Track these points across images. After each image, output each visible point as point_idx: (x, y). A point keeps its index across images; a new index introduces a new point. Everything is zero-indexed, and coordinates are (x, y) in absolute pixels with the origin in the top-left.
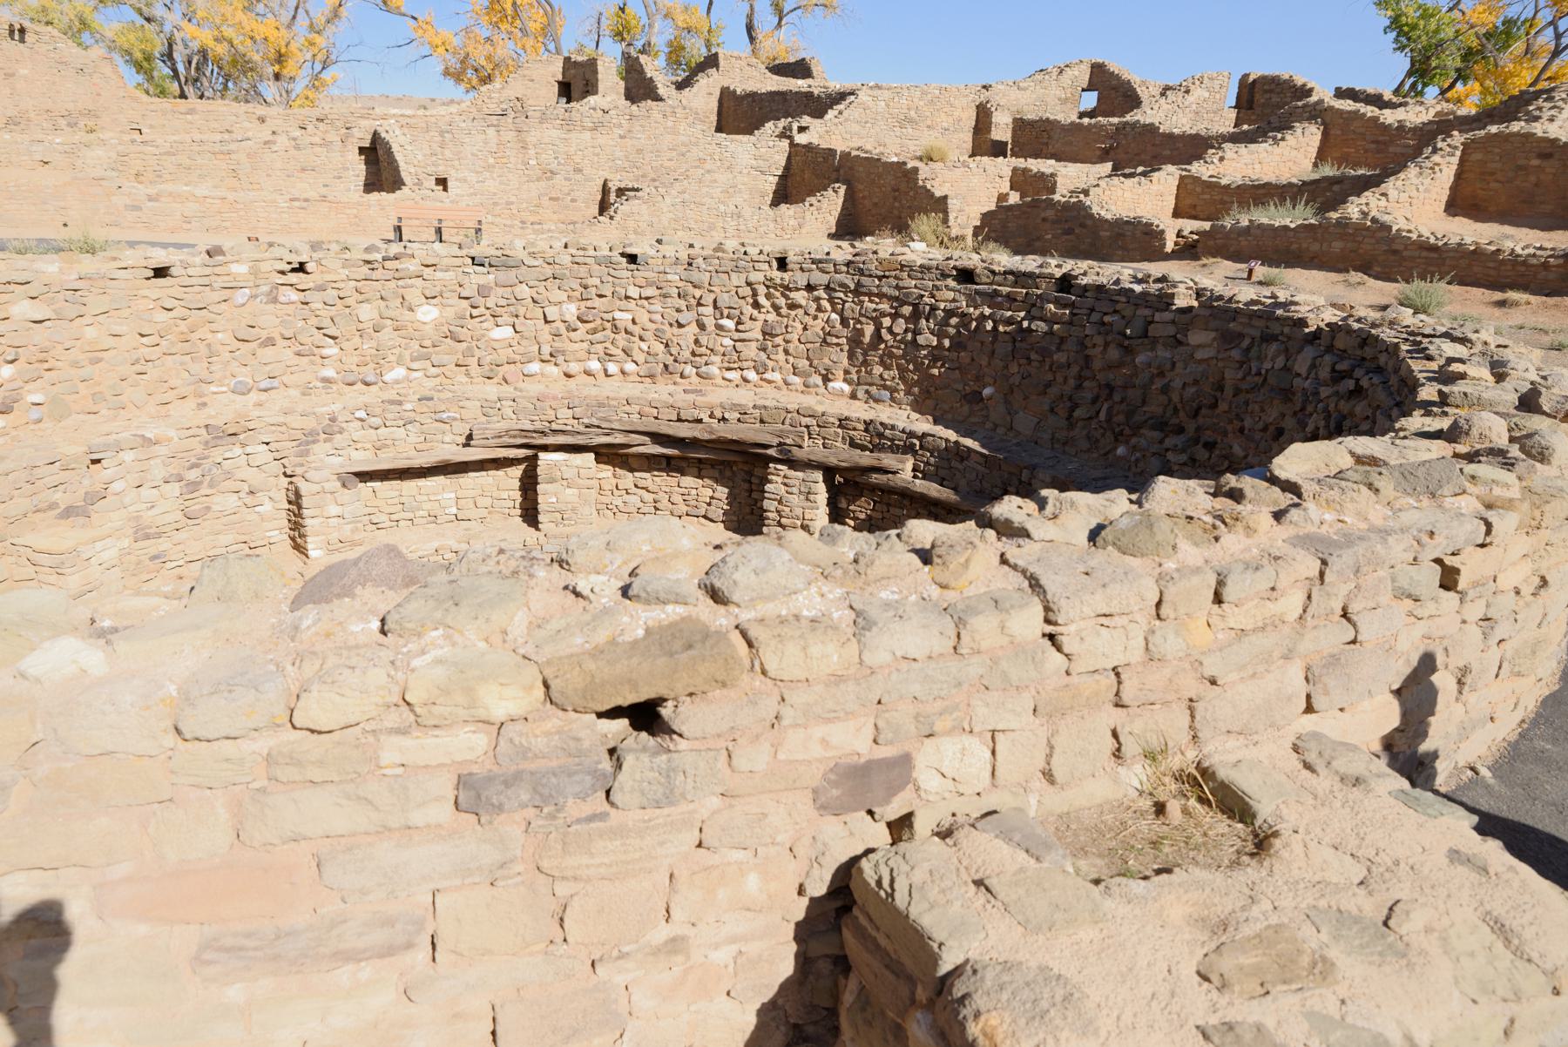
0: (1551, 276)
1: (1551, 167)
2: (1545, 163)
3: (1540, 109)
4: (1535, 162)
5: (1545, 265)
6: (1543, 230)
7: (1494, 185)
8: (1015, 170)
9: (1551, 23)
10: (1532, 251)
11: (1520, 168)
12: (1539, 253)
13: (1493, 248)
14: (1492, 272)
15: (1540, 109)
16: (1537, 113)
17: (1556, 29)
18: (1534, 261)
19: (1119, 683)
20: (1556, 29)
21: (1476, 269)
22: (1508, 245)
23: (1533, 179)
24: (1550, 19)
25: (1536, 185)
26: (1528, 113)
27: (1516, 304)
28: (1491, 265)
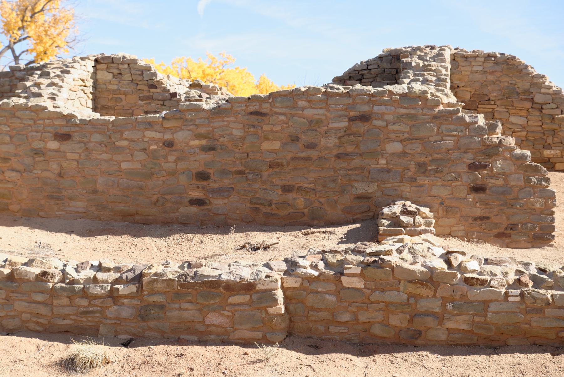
0: (126, 313)
1: (72, 149)
2: (66, 146)
3: (38, 85)
4: (53, 145)
5: (113, 295)
6: (82, 235)
7: (10, 175)
8: (542, 236)
9: (9, 47)
10: (90, 273)
11: (37, 152)
12: (101, 276)
13: (35, 270)
14: (43, 310)
15: (38, 85)
16: (35, 90)
17: (13, 51)
18: (96, 290)
19: (23, 52)
20: (13, 51)
21: (20, 306)
22: (54, 265)
23: (54, 166)
24: (7, 44)
25: (60, 175)
26: (26, 89)
27: (91, 364)
28: (39, 298)
